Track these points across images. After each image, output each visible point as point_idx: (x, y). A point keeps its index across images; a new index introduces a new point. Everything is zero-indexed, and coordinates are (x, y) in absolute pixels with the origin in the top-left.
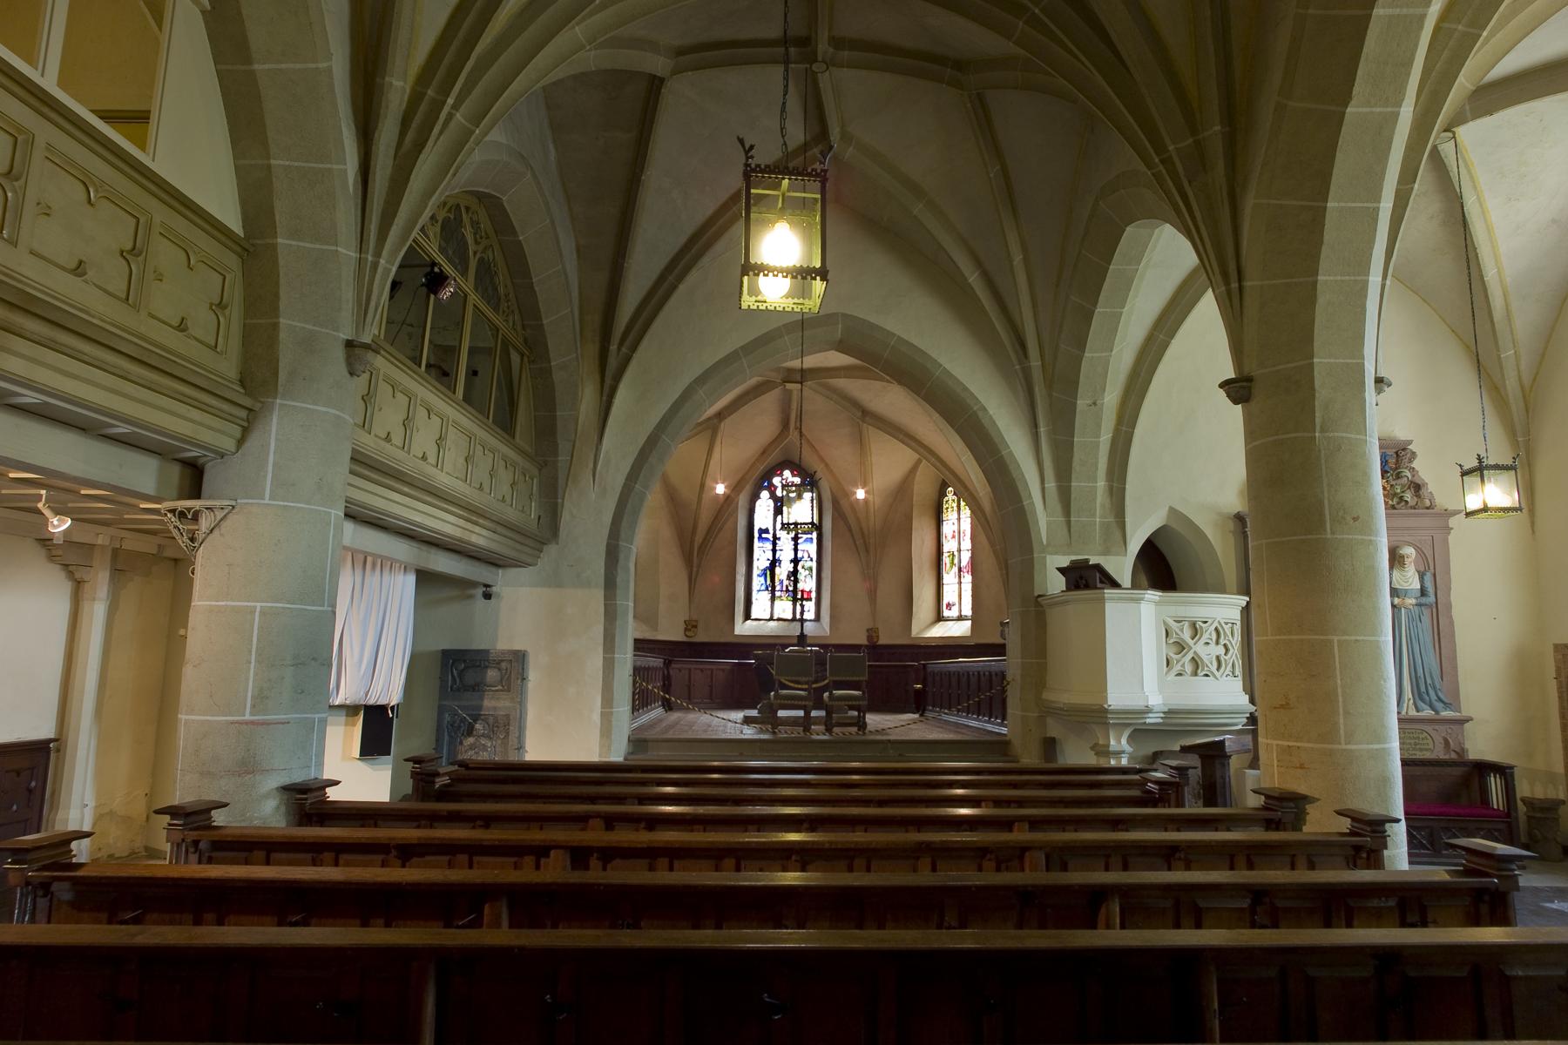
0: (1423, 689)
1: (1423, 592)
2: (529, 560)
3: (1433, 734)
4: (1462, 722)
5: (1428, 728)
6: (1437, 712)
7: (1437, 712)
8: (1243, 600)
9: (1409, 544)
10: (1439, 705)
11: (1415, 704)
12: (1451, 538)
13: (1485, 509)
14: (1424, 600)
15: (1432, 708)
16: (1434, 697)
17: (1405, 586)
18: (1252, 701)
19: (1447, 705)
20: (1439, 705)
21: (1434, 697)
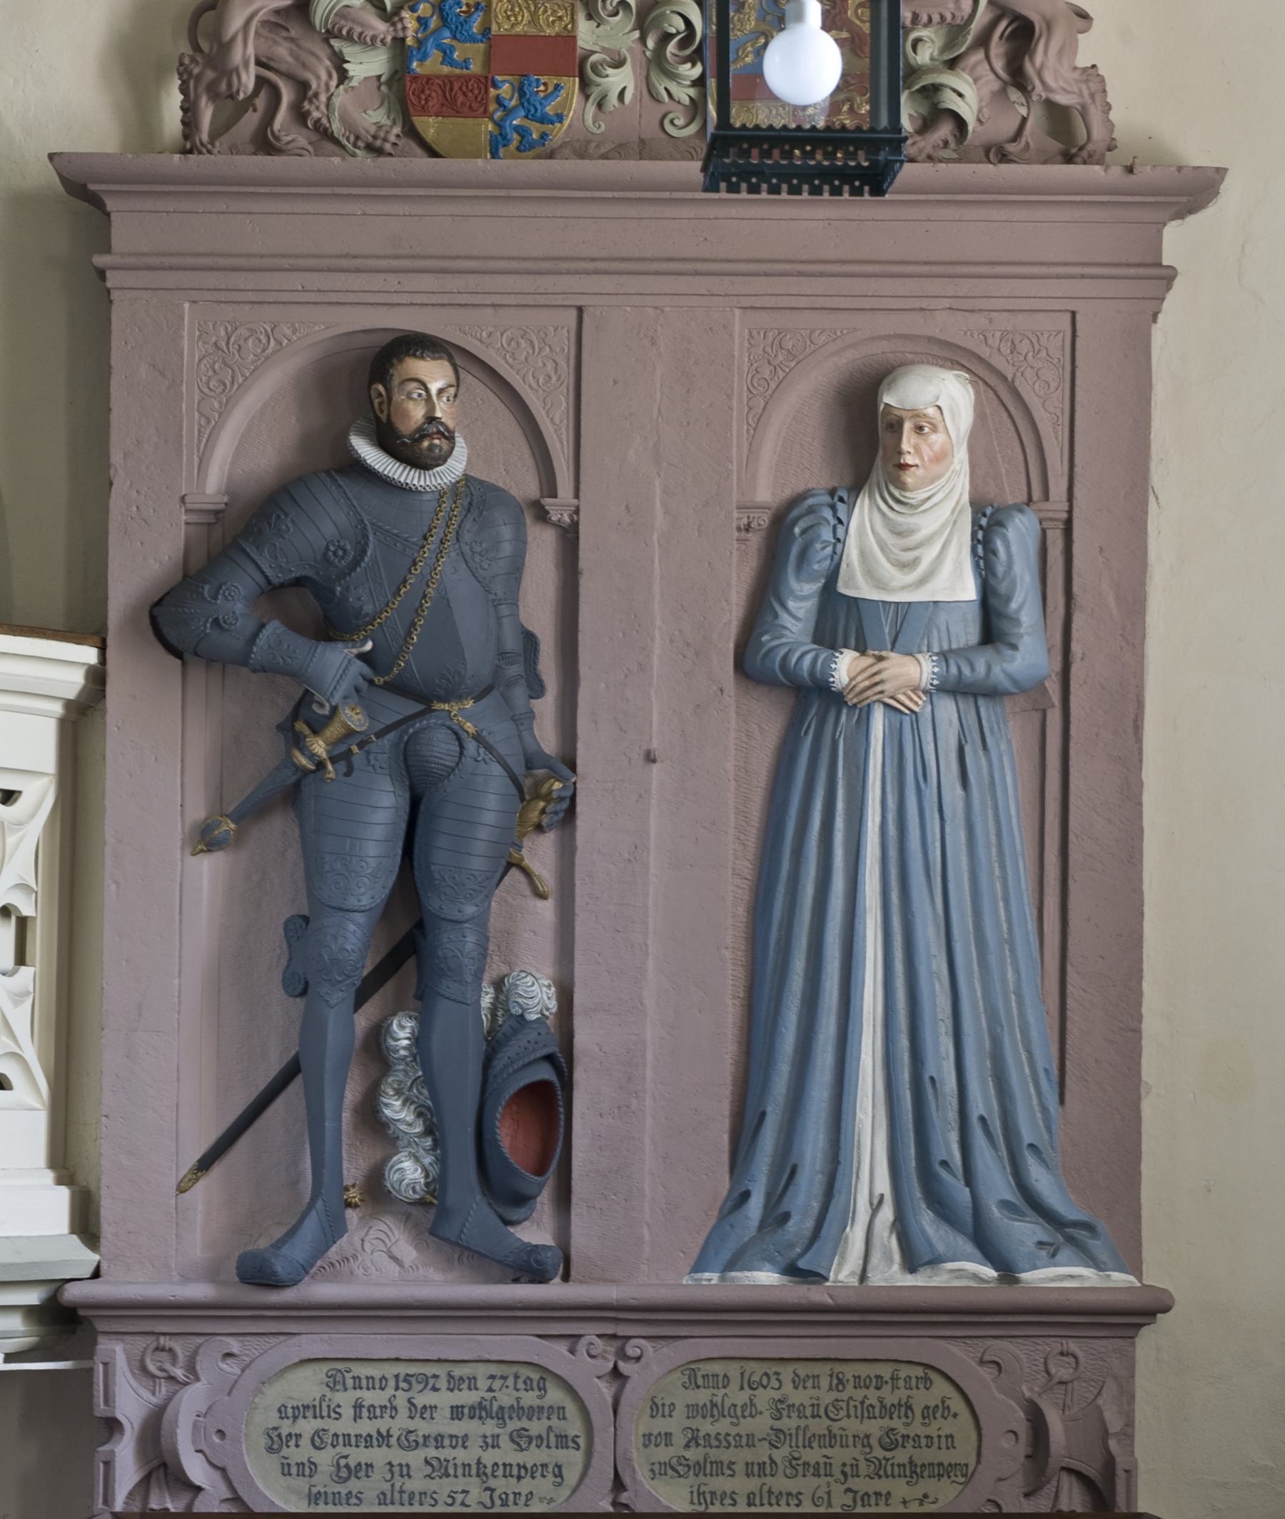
0: (947, 1144)
1: (992, 623)
2: (1103, 1256)
3: (980, 1381)
4: (1129, 1318)
5: (956, 1354)
6: (1008, 1273)
7: (1008, 1273)
8: (89, 655)
9: (952, 355)
10: (1023, 1233)
11: (901, 1226)
12: (1166, 337)
13: (111, 302)
14: (982, 666)
15: (987, 1247)
16: (996, 1183)
17: (899, 588)
18: (86, 1223)
19: (1068, 1235)
20: (1023, 1233)
21: (996, 1183)
